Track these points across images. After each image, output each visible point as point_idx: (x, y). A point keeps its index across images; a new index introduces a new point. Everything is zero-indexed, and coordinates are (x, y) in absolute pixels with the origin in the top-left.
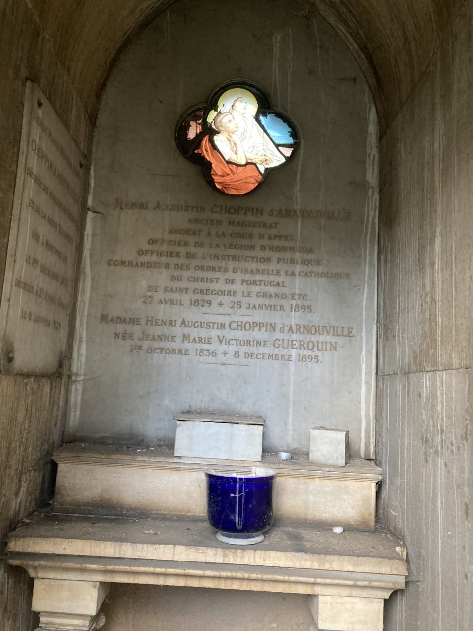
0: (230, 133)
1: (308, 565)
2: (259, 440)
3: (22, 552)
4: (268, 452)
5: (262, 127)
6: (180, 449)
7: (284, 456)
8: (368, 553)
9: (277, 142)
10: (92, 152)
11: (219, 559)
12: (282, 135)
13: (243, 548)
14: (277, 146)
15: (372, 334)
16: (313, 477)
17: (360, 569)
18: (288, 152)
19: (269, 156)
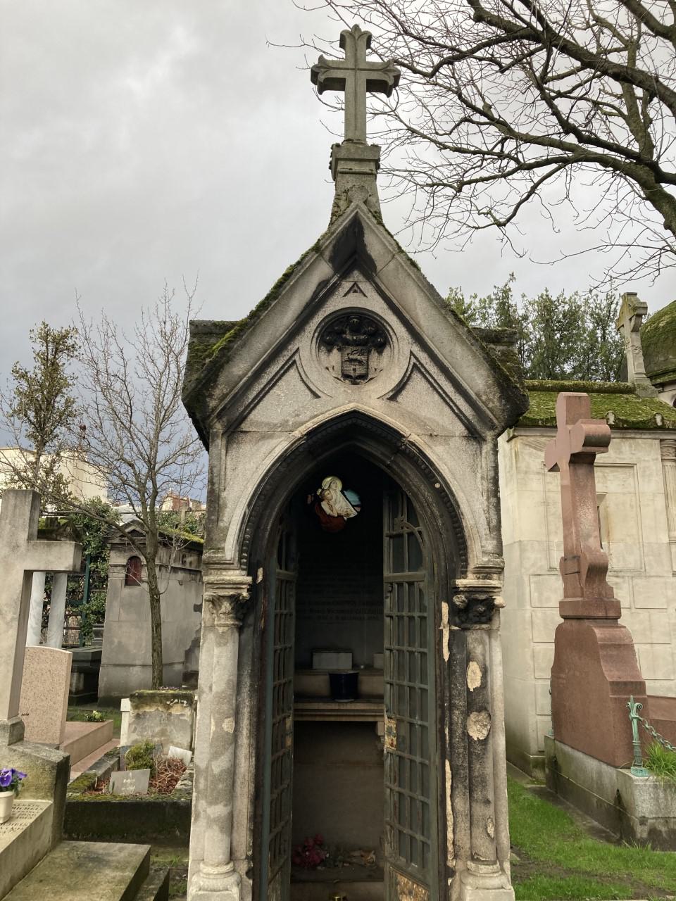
0: (329, 500)
1: (372, 708)
2: (351, 659)
3: (109, 706)
4: (355, 666)
5: (345, 496)
6: (316, 665)
7: (362, 667)
8: (483, 160)
9: (353, 504)
10: (190, 417)
11: (337, 708)
12: (354, 498)
13: (346, 703)
14: (353, 506)
15: (403, 553)
16: (374, 675)
17: (465, 838)
18: (359, 509)
19: (349, 512)
